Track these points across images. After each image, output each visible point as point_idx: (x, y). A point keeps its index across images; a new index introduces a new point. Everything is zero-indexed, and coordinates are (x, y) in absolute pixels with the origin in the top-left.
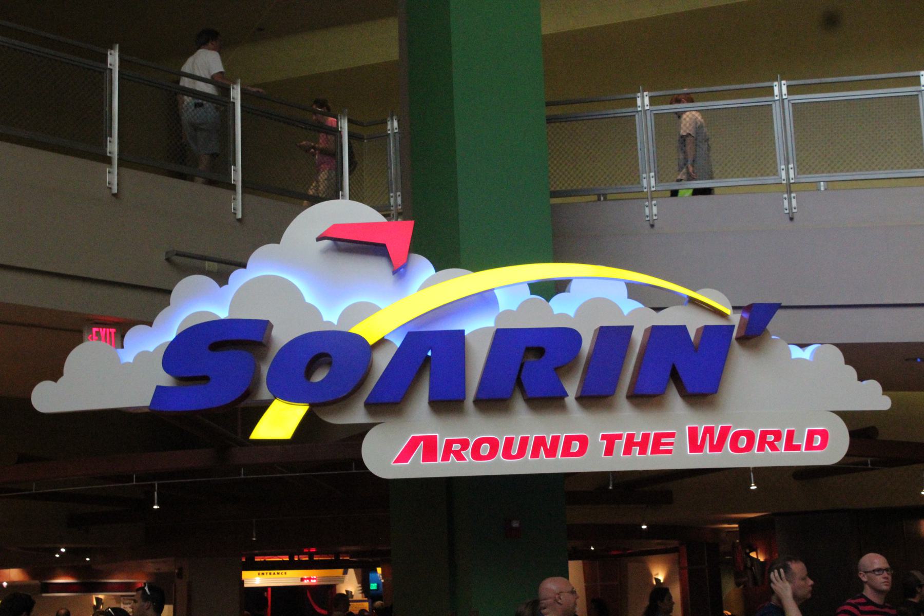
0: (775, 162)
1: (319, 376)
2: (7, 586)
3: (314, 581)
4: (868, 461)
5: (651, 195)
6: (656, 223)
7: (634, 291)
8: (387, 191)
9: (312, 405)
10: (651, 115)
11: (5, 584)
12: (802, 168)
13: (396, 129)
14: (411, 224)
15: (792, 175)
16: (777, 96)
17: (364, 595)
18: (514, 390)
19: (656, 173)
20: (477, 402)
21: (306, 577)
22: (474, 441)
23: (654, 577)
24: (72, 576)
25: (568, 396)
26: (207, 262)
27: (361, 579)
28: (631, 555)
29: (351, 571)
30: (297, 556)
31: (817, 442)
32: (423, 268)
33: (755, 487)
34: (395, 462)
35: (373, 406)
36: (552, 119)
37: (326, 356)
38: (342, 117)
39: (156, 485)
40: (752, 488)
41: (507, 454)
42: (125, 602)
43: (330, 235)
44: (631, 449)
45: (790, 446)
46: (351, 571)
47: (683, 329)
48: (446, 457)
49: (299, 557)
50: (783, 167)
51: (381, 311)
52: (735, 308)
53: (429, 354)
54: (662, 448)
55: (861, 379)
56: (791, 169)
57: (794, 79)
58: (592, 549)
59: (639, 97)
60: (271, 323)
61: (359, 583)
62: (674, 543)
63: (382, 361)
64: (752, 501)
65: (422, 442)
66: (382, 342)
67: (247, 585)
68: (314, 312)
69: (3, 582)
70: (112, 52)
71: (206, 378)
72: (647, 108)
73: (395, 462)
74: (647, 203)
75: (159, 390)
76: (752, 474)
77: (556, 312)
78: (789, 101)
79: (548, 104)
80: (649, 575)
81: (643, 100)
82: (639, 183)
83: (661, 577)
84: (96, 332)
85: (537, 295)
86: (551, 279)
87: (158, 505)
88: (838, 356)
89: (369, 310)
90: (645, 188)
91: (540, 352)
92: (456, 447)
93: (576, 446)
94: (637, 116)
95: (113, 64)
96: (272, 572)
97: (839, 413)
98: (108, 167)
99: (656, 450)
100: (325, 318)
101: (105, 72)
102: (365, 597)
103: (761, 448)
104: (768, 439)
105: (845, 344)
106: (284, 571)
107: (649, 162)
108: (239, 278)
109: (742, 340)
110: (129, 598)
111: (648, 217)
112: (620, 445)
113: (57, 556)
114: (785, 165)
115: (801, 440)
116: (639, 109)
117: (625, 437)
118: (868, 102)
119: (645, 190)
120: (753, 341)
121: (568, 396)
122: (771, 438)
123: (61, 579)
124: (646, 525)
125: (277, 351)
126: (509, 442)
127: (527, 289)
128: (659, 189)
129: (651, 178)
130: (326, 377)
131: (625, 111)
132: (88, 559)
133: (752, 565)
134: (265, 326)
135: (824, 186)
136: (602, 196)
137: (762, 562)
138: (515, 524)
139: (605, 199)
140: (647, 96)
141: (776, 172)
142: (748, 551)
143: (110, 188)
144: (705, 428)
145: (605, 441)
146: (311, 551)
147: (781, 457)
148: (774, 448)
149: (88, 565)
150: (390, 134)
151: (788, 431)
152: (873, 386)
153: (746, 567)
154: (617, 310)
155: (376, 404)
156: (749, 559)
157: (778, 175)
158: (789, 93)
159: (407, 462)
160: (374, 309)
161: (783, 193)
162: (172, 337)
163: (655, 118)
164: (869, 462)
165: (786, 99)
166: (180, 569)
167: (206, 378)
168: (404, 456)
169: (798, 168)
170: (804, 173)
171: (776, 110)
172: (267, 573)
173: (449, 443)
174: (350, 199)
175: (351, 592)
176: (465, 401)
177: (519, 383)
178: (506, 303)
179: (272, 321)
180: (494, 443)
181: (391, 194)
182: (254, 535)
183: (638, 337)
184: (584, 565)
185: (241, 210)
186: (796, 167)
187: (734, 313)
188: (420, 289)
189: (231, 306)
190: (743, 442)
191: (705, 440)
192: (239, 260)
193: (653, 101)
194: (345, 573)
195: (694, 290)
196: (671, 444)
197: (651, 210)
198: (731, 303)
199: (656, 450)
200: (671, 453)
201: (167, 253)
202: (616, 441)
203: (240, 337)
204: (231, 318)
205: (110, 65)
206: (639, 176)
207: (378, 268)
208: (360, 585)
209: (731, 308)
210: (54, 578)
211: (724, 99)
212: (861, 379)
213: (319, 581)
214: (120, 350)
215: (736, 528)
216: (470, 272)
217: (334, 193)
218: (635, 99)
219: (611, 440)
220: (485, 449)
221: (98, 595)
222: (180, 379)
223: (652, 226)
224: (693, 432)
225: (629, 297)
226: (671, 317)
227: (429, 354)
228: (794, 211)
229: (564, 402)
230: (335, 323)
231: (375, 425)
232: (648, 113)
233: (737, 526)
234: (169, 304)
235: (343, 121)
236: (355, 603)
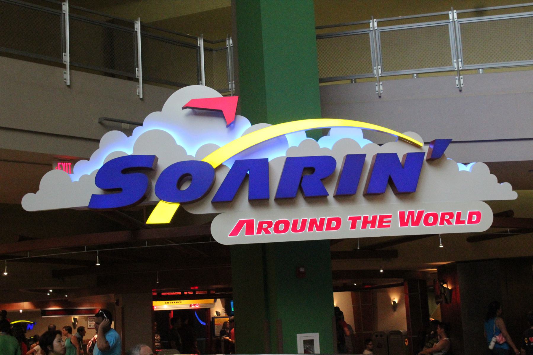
0: (451, 58)
1: (185, 187)
2: (22, 312)
3: (197, 307)
4: (508, 230)
5: (379, 79)
6: (382, 95)
7: (367, 134)
8: (227, 81)
9: (181, 204)
10: (378, 32)
11: (21, 311)
12: (466, 61)
13: (231, 44)
14: (237, 97)
15: (460, 65)
16: (451, 19)
17: (226, 314)
18: (297, 194)
19: (382, 67)
20: (277, 199)
21: (192, 304)
22: (275, 222)
23: (392, 300)
24: (59, 306)
25: (329, 195)
26: (123, 124)
27: (224, 305)
28: (376, 288)
29: (219, 300)
30: (186, 292)
31: (474, 219)
32: (244, 123)
33: (442, 246)
34: (229, 236)
35: (216, 203)
36: (323, 36)
37: (187, 176)
38: (200, 38)
39: (98, 252)
40: (440, 247)
41: (294, 229)
42: (90, 320)
43: (188, 106)
44: (366, 225)
45: (458, 221)
46: (219, 300)
47: (395, 155)
48: (259, 232)
49: (187, 293)
50: (455, 61)
51: (219, 149)
52: (425, 143)
53: (248, 173)
54: (384, 224)
55: (500, 181)
56: (460, 61)
57: (380, 18)
58: (355, 285)
59: (371, 22)
60: (157, 157)
61: (223, 307)
62: (401, 280)
63: (221, 177)
64: (441, 255)
65: (245, 224)
66: (221, 166)
67: (156, 309)
69: (20, 310)
70: (65, 3)
71: (120, 190)
72: (376, 28)
73: (229, 236)
74: (377, 84)
76: (440, 239)
77: (321, 147)
78: (458, 22)
79: (317, 28)
80: (389, 299)
82: (372, 72)
83: (396, 300)
84: (60, 165)
85: (314, 139)
86: (320, 127)
87: (99, 263)
88: (487, 169)
89: (212, 148)
90: (376, 75)
91: (312, 170)
93: (334, 224)
94: (370, 33)
95: (65, 10)
96: (173, 301)
97: (486, 202)
98: (65, 70)
99: (380, 225)
100: (188, 154)
101: (60, 16)
102: (227, 315)
103: (442, 223)
104: (446, 218)
106: (180, 301)
107: (377, 59)
108: (138, 132)
109: (428, 160)
110: (93, 318)
111: (377, 92)
112: (360, 223)
113: (48, 294)
114: (456, 59)
115: (465, 218)
116: (371, 29)
118: (482, 23)
119: (376, 76)
121: (329, 195)
122: (447, 217)
123: (53, 308)
124: (382, 270)
125: (161, 172)
126: (295, 222)
127: (305, 134)
128: (383, 75)
129: (379, 69)
130: (189, 188)
131: (363, 30)
132: (66, 296)
133: (444, 292)
134: (153, 159)
135: (482, 71)
136: (353, 80)
137: (450, 290)
138: (302, 270)
139: (355, 82)
140: (375, 21)
141: (451, 64)
142: (442, 284)
143: (66, 82)
144: (409, 212)
145: (351, 221)
146: (195, 288)
147: (453, 228)
148: (449, 223)
149: (66, 300)
150: (228, 47)
151: (458, 213)
152: (507, 186)
153: (441, 293)
154: (358, 145)
155: (218, 202)
156: (442, 288)
157: (452, 66)
158: (458, 17)
159: (237, 235)
160: (217, 147)
161: (456, 76)
162: (99, 167)
163: (381, 34)
164: (509, 231)
165: (456, 21)
167: (120, 190)
168: (235, 232)
169: (464, 61)
170: (467, 64)
171: (451, 27)
172: (170, 302)
173: (261, 224)
174: (205, 86)
175: (219, 312)
176: (270, 199)
177: (300, 188)
178: (293, 142)
179: (157, 156)
180: (287, 223)
181: (230, 82)
182: (158, 280)
183: (369, 160)
185: (142, 93)
186: (462, 60)
187: (425, 146)
188: (243, 135)
189: (134, 148)
190: (431, 220)
191: (409, 220)
192: (139, 122)
193: (379, 24)
194: (215, 301)
195: (402, 132)
196: (389, 222)
197: (379, 87)
198: (424, 140)
199: (380, 225)
200: (389, 227)
201: (99, 119)
202: (357, 220)
203: (140, 165)
204: (134, 155)
205: (64, 11)
206: (372, 68)
207: (219, 124)
208: (224, 308)
210: (49, 307)
211: (399, 24)
212: (500, 181)
213: (200, 306)
214: (71, 175)
215: (436, 271)
216: (271, 125)
217: (198, 82)
219: (354, 220)
220: (282, 227)
221: (75, 316)
222: (106, 190)
223: (380, 97)
224: (402, 214)
226: (388, 149)
227: (248, 173)
228: (462, 86)
229: (327, 198)
230: (194, 156)
231: (217, 215)
232: (376, 31)
233: (436, 269)
234: (98, 148)
235: (200, 40)
236: (221, 319)
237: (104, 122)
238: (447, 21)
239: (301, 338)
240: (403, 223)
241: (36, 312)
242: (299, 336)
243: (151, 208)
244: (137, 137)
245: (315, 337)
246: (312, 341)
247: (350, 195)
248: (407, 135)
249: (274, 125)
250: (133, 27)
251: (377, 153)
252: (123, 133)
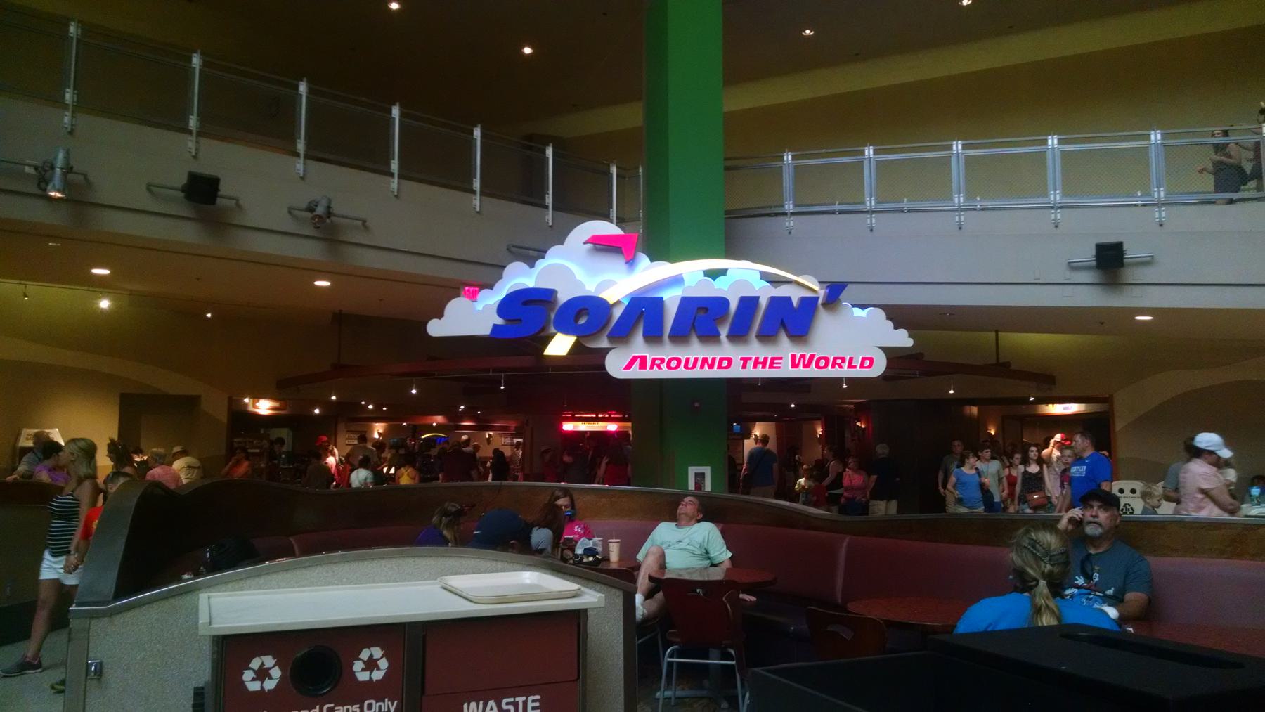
0: (864, 195)
1: (582, 321)
7: (764, 276)
11: (434, 424)
32: (643, 260)
41: (686, 367)
45: (850, 366)
47: (788, 299)
48: (652, 368)
50: (868, 199)
54: (775, 365)
55: (896, 328)
63: (617, 313)
66: (619, 302)
71: (520, 320)
72: (790, 162)
75: (495, 326)
81: (788, 157)
88: (881, 314)
92: (658, 362)
93: (725, 363)
97: (880, 347)
99: (771, 367)
101: (472, 141)
105: (888, 306)
108: (541, 264)
112: (750, 364)
115: (857, 363)
117: (753, 359)
122: (839, 361)
126: (688, 360)
127: (703, 274)
131: (778, 163)
148: (840, 367)
166: (527, 421)
168: (628, 367)
173: (654, 360)
183: (763, 302)
184: (777, 427)
189: (536, 279)
190: (822, 363)
193: (794, 158)
207: (618, 262)
209: (818, 283)
212: (896, 328)
218: (783, 156)
219: (745, 360)
220: (674, 363)
222: (507, 320)
223: (790, 233)
224: (793, 357)
226: (782, 291)
230: (593, 291)
237: (513, 249)
238: (862, 157)
239: (692, 471)
240: (794, 366)
241: (451, 426)
242: (709, 468)
243: (547, 340)
245: (707, 470)
246: (703, 474)
247: (742, 336)
248: (806, 280)
249: (672, 263)
250: (544, 153)
251: (770, 296)
252: (527, 266)
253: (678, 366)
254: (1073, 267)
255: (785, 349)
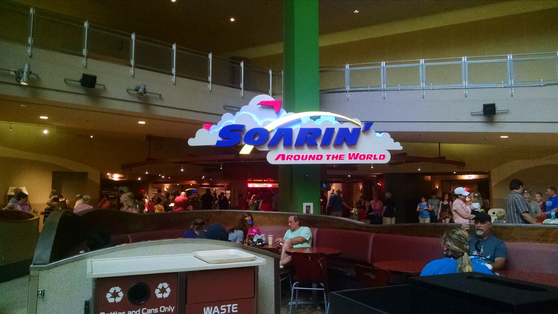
1: (256, 139)
7: (336, 119)
11: (191, 185)
35: (269, 146)
41: (302, 159)
47: (348, 129)
48: (287, 159)
54: (341, 158)
55: (395, 142)
57: (351, 64)
62: (361, 180)
63: (272, 135)
66: (272, 131)
68: (256, 123)
88: (388, 135)
92: (290, 157)
93: (319, 157)
94: (346, 71)
99: (340, 159)
101: (208, 60)
104: (369, 157)
108: (238, 114)
112: (331, 157)
115: (378, 157)
120: (366, 132)
122: (370, 156)
126: (303, 156)
131: (343, 69)
138: (307, 176)
148: (290, 159)
152: (398, 144)
168: (277, 159)
173: (288, 156)
177: (305, 141)
180: (299, 156)
183: (336, 131)
190: (362, 157)
207: (273, 112)
210: (204, 183)
212: (395, 142)
218: (345, 66)
219: (328, 156)
220: (297, 158)
224: (350, 154)
225: (335, 120)
226: (345, 126)
230: (261, 125)
234: (221, 120)
237: (227, 107)
239: (305, 205)
240: (350, 158)
241: (198, 185)
242: (312, 204)
243: (241, 147)
244: (238, 116)
245: (311, 204)
253: (299, 159)
254: (473, 114)
255: (346, 150)
